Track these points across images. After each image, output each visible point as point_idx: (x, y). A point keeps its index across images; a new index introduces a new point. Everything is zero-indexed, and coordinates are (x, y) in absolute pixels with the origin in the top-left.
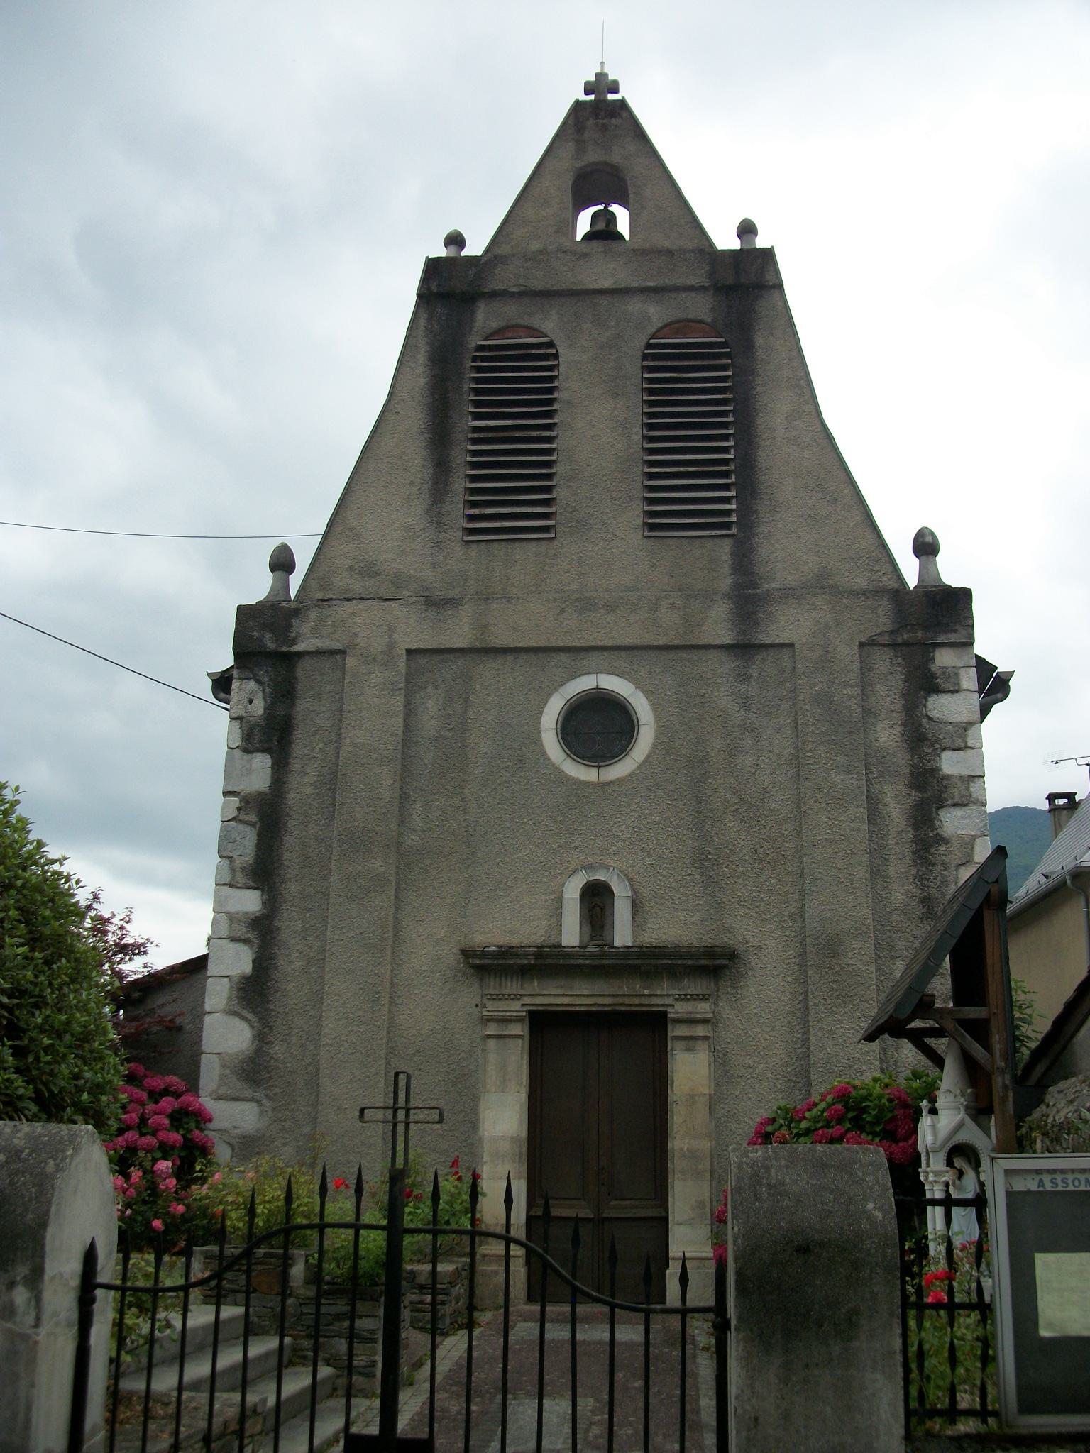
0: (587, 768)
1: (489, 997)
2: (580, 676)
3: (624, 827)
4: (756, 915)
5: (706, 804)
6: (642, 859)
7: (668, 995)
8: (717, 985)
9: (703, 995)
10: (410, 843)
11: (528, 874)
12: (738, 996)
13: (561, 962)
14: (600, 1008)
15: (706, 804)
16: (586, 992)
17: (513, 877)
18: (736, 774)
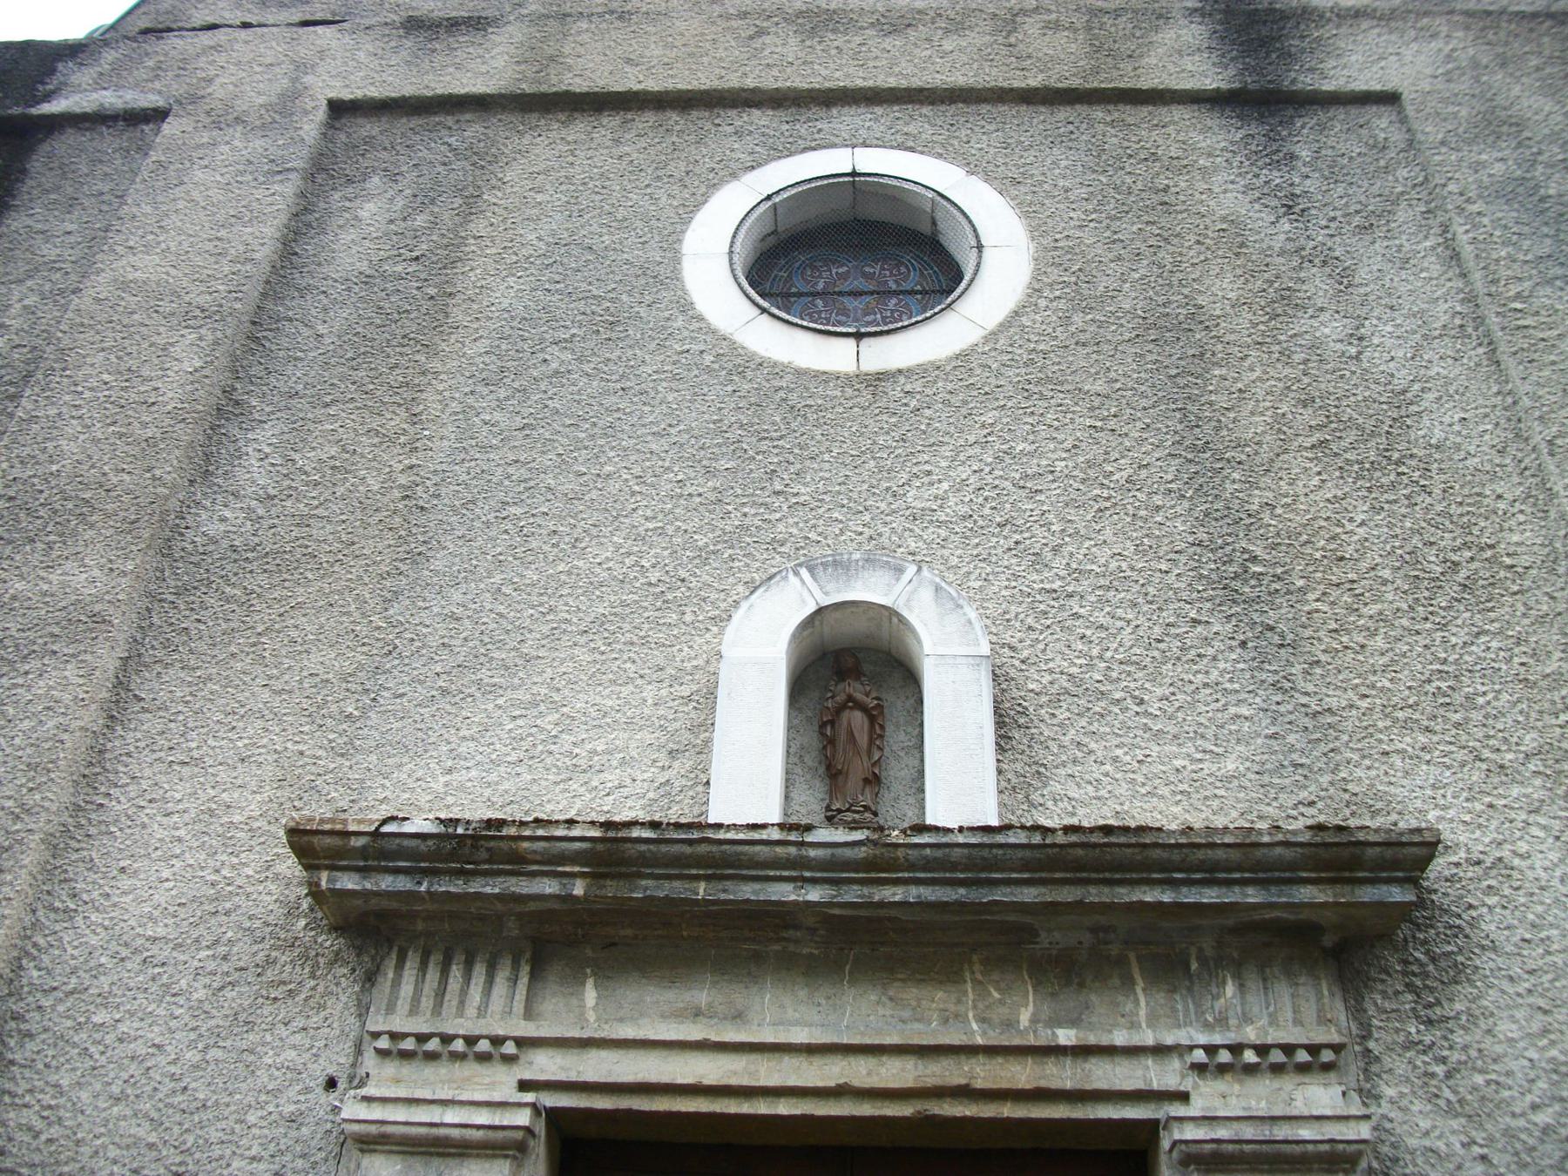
0: (820, 339)
1: (383, 1043)
2: (805, 150)
3: (945, 486)
4: (1461, 755)
5: (1217, 429)
6: (1016, 577)
7: (1160, 1051)
8: (1357, 1011)
9: (1313, 1049)
10: (215, 529)
11: (601, 620)
12: (1455, 1056)
13: (702, 890)
14: (866, 1109)
15: (1217, 429)
16: (800, 1036)
17: (545, 629)
18: (1297, 358)
